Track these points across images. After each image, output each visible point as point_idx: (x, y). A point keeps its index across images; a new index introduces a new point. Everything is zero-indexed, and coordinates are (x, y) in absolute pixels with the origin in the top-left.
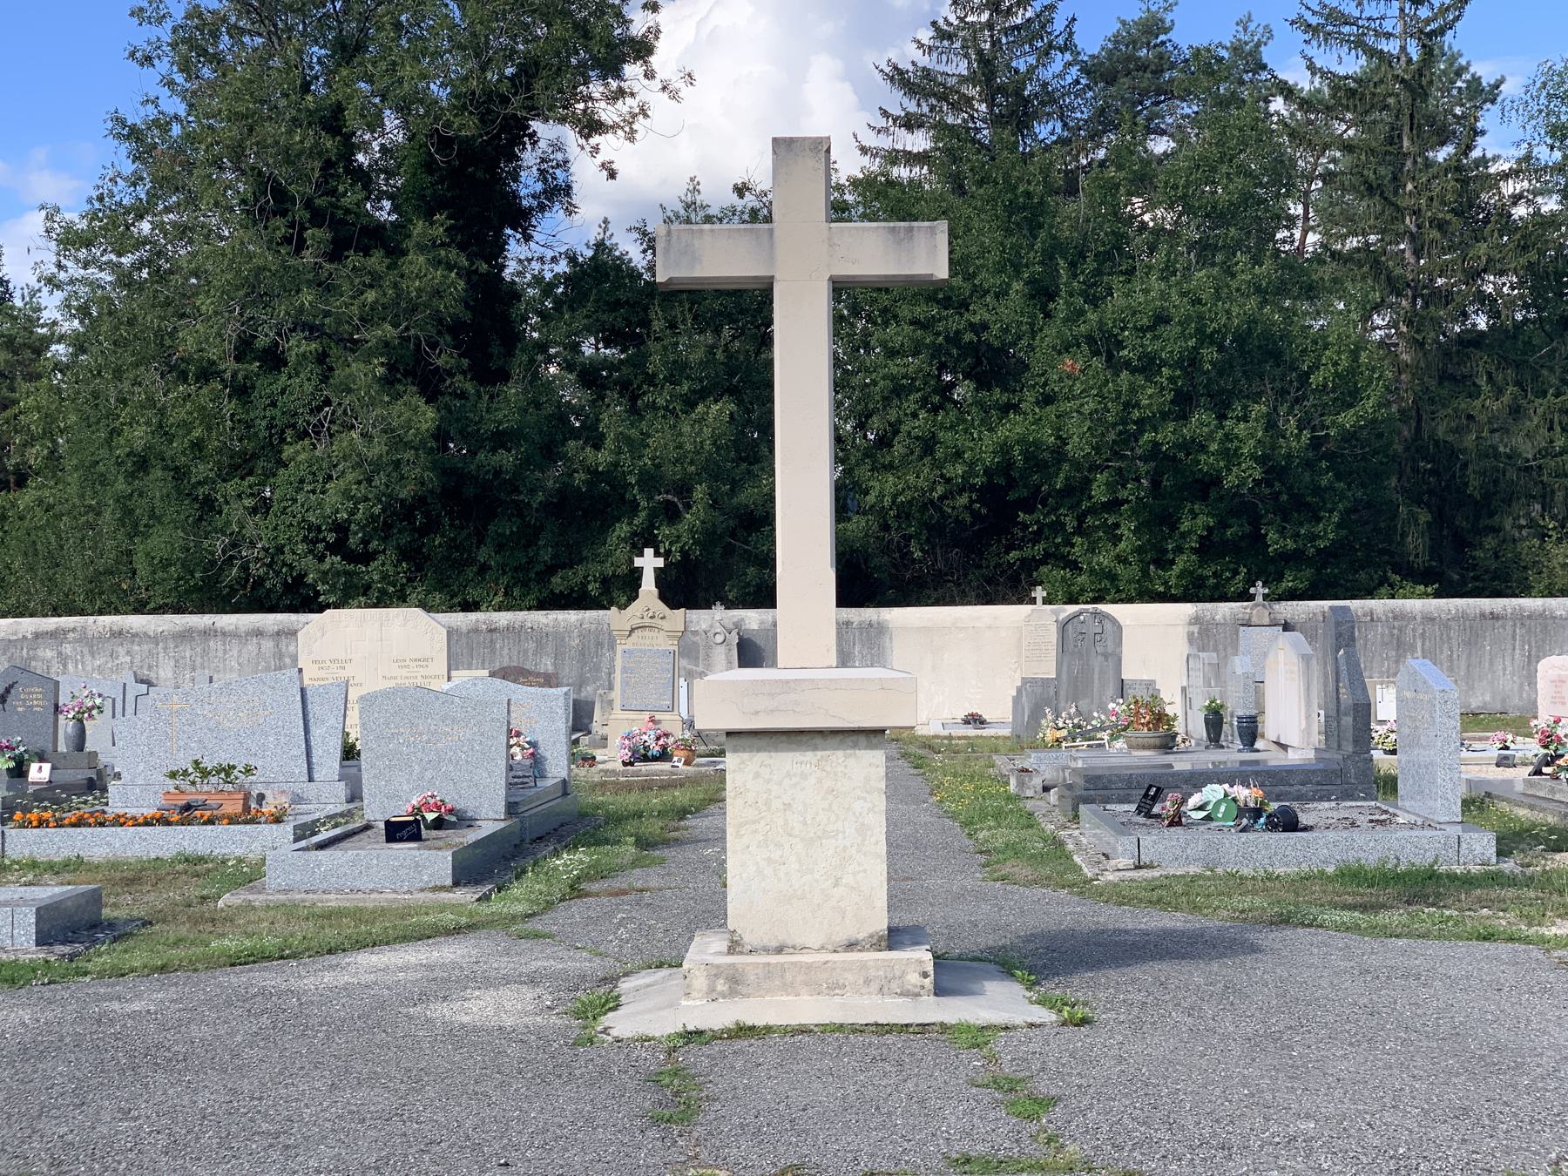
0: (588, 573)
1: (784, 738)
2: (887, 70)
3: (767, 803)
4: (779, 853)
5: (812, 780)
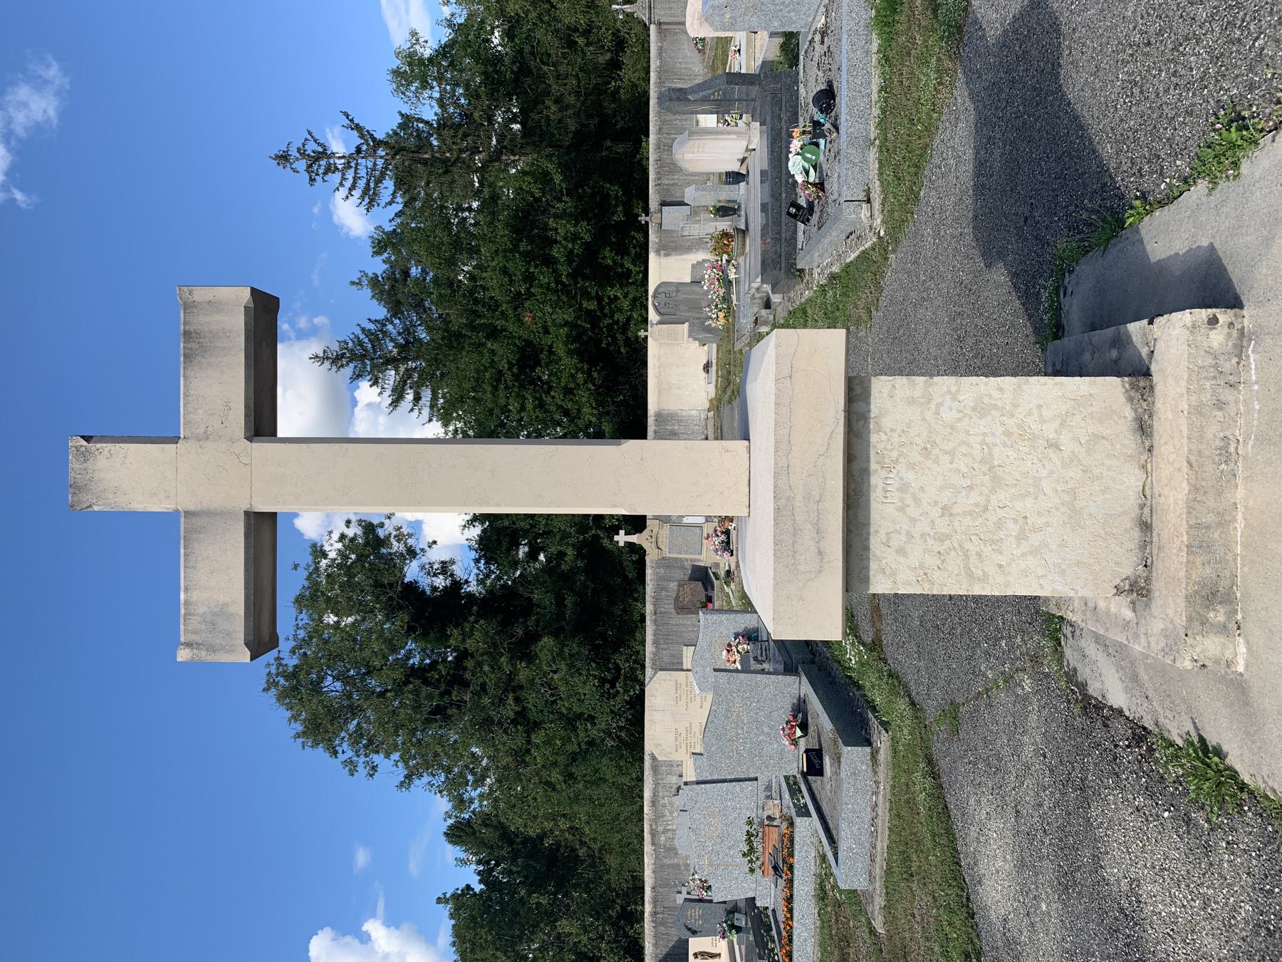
3: (941, 538)
4: (1010, 525)
5: (910, 476)
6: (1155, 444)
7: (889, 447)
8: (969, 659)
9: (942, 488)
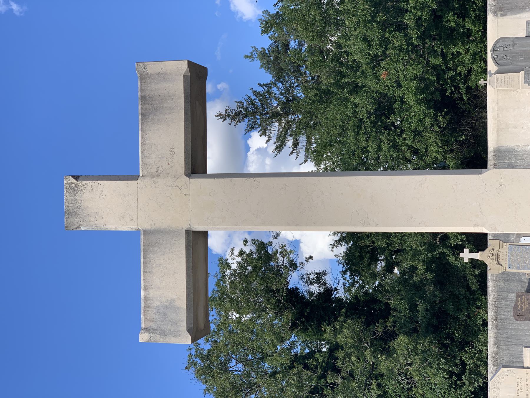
0: (471, 274)
2: (276, 153)
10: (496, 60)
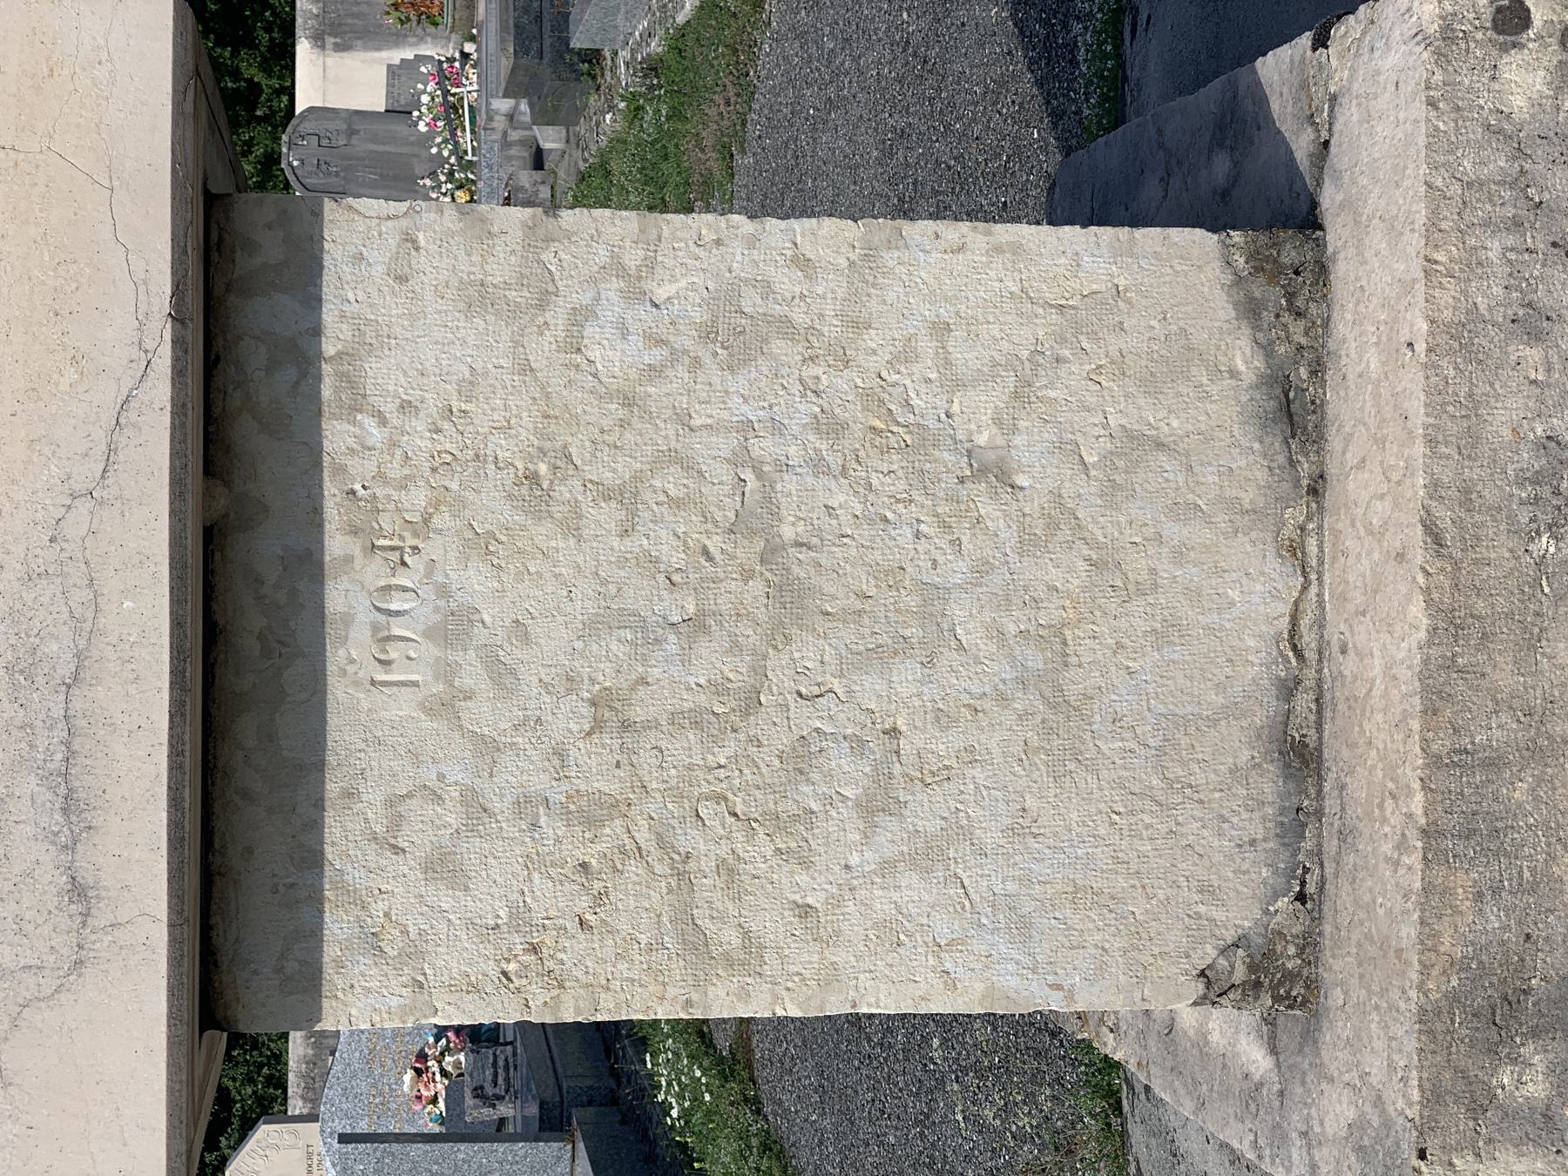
1: (246, 729)
3: (590, 814)
4: (840, 760)
5: (474, 582)
6: (1332, 469)
7: (395, 471)
8: (924, 1120)
9: (594, 627)
10: (299, 173)
